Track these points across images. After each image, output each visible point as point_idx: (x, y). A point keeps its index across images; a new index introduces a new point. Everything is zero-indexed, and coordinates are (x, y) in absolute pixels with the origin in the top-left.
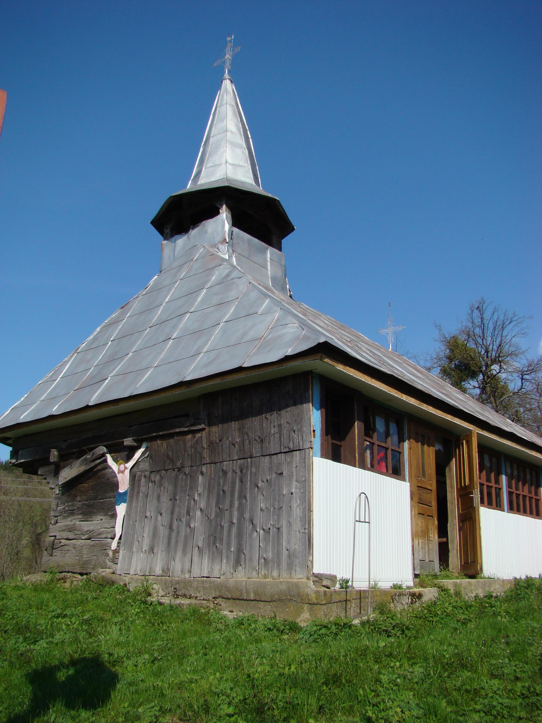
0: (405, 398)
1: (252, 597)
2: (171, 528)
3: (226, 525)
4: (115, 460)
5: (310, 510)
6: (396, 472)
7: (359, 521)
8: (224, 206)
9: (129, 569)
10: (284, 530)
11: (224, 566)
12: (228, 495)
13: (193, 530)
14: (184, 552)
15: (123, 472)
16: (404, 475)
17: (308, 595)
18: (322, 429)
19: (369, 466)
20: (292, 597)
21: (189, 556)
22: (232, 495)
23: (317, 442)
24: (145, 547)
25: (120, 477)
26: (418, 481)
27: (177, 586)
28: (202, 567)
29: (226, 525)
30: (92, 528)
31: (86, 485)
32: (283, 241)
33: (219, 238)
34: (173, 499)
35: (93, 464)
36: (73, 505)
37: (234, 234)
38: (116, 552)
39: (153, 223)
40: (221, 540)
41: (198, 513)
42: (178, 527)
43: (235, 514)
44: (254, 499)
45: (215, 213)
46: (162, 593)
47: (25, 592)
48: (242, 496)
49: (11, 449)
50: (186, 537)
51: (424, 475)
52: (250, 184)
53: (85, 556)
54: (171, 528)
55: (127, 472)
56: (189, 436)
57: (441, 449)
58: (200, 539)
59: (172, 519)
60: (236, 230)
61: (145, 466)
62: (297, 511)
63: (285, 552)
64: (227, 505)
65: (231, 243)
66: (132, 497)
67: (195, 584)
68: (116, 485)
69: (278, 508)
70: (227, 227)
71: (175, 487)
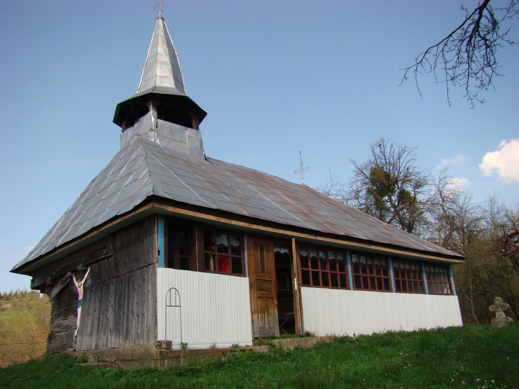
0: (234, 222)
1: (130, 358)
2: (99, 320)
3: (122, 314)
4: (77, 280)
5: (156, 302)
6: (237, 270)
7: (170, 306)
8: (151, 107)
9: (81, 348)
10: (145, 314)
11: (121, 340)
12: (123, 296)
13: (108, 319)
14: (105, 334)
15: (80, 287)
16: (245, 273)
17: (153, 354)
18: (165, 250)
19: (212, 269)
20: (146, 356)
21: (106, 336)
22: (125, 296)
23: (162, 258)
24: (89, 333)
25: (79, 289)
26: (257, 276)
27: (99, 355)
28: (113, 342)
29: (122, 314)
30: (68, 324)
31: (65, 297)
32: (200, 126)
33: (149, 128)
34: (100, 301)
35: (65, 284)
36: (60, 310)
37: (159, 124)
38: (76, 337)
39: (115, 121)
40: (120, 324)
41: (111, 308)
42: (102, 318)
43: (126, 307)
44: (133, 297)
45: (147, 111)
46: (93, 360)
47: (236, 353)
48: (129, 297)
49: (31, 278)
50: (106, 324)
51: (263, 271)
52: (171, 88)
53: (64, 342)
54: (99, 320)
55: (82, 286)
56: (106, 261)
57: (287, 252)
58: (111, 324)
59: (100, 314)
60: (160, 121)
61: (89, 282)
62: (151, 302)
63: (146, 329)
64: (122, 303)
65: (156, 130)
66: (83, 302)
67: (106, 353)
68: (77, 295)
69: (143, 302)
70: (153, 119)
71: (102, 293)
